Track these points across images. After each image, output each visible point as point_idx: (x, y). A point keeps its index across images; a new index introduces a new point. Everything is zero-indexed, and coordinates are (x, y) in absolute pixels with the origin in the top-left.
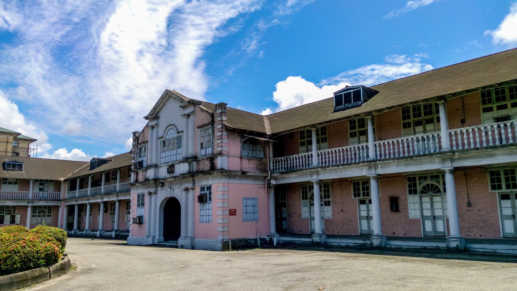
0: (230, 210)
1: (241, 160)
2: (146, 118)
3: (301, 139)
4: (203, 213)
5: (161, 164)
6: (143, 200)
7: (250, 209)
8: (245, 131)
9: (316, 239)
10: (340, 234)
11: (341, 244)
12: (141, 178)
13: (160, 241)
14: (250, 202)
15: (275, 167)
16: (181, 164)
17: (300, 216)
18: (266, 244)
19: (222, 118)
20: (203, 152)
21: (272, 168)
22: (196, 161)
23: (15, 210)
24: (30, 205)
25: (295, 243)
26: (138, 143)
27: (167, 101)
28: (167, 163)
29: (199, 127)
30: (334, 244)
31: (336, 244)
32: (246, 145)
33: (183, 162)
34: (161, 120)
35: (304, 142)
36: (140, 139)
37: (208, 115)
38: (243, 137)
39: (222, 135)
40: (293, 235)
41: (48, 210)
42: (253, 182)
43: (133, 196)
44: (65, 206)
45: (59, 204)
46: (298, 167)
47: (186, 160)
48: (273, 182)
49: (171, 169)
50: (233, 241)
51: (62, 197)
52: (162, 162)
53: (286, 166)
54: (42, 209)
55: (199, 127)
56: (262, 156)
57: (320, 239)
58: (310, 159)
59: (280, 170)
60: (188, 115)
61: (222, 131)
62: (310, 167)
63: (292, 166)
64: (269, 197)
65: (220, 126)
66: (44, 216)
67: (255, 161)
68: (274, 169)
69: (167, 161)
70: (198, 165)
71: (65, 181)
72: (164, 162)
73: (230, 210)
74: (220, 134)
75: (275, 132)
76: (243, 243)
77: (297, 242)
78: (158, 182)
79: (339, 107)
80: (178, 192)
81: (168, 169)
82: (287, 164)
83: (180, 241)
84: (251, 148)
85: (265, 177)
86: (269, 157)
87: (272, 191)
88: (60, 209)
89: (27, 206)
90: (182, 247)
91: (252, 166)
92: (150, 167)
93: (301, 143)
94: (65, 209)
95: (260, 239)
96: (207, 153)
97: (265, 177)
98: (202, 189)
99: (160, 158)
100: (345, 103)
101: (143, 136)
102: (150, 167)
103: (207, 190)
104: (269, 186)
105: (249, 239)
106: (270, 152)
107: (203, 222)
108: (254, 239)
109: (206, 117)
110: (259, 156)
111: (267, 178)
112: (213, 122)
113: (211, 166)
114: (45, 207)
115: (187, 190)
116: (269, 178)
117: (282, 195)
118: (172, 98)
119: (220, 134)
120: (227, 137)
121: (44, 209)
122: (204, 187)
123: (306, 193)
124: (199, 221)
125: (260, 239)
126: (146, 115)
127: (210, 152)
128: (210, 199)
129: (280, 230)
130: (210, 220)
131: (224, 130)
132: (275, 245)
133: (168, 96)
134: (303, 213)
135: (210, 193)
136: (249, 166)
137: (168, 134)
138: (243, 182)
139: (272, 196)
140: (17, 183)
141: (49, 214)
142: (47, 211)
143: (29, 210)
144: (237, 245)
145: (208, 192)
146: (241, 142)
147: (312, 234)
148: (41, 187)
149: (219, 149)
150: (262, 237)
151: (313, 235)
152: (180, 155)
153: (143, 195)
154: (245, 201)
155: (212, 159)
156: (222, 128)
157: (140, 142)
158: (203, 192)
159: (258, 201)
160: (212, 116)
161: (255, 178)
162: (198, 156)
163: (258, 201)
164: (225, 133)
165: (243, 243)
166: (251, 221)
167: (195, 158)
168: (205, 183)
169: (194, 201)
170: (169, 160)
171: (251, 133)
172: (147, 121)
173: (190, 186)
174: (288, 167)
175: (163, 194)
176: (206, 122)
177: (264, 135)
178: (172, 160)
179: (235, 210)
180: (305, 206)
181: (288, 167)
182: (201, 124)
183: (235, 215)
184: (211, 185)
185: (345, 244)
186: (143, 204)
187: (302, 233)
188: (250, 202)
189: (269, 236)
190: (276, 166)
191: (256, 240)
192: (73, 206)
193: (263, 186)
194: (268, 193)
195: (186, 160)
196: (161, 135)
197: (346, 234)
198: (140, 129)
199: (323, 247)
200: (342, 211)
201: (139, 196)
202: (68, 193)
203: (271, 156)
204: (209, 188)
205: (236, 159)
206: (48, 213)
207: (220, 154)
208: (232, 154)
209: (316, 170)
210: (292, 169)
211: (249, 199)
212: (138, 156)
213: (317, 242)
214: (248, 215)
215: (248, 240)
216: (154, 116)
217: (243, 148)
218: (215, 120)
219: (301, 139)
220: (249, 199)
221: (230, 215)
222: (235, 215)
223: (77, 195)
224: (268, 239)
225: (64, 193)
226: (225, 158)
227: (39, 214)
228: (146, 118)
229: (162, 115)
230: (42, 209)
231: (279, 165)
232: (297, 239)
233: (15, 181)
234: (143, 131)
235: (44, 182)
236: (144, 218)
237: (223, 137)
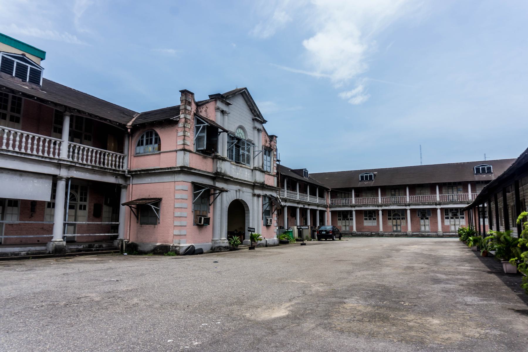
88: (326, 213)
94: (330, 214)
225: (328, 201)
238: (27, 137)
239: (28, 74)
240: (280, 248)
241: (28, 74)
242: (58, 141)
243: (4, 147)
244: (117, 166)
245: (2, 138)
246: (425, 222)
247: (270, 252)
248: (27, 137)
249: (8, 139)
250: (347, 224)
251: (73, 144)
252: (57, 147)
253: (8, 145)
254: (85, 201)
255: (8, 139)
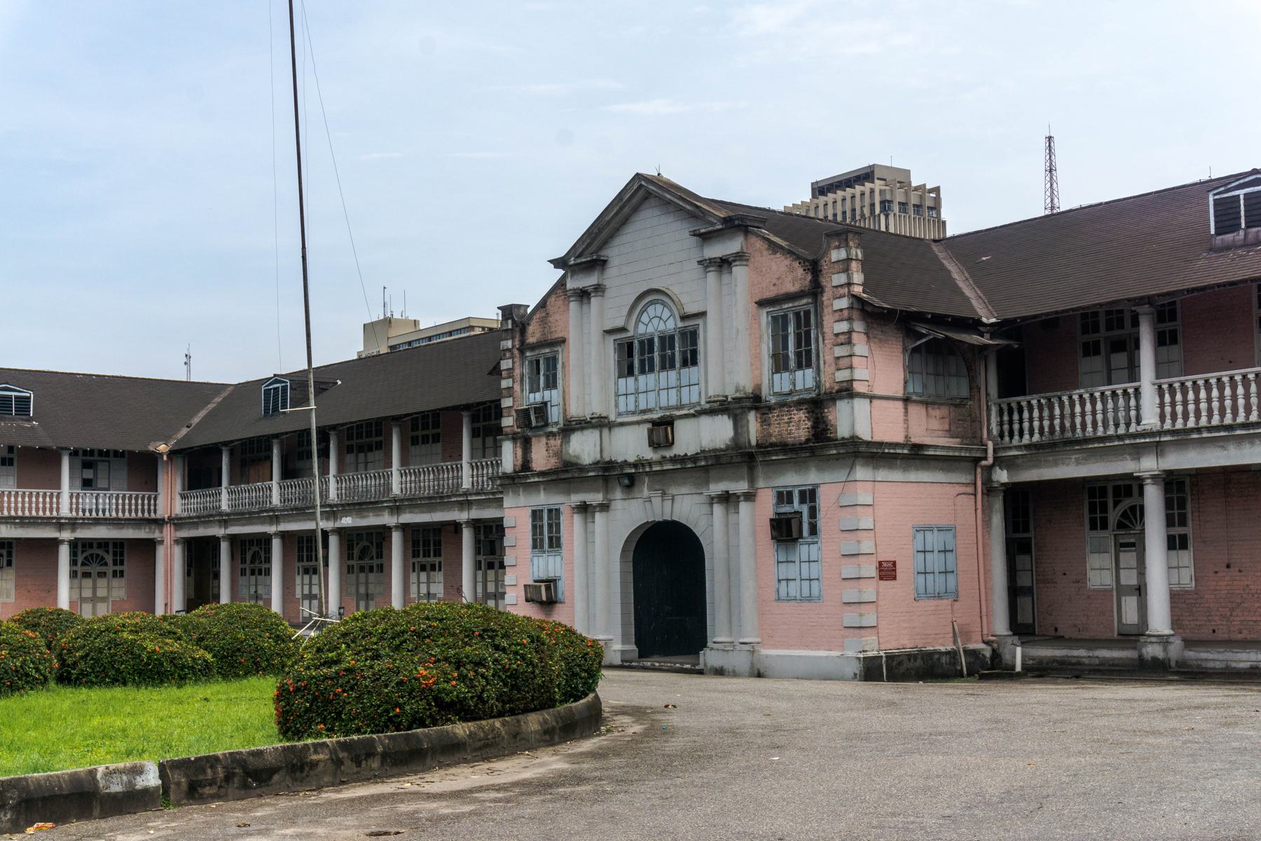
0: (880, 563)
1: (906, 409)
2: (558, 263)
3: (1085, 331)
4: (791, 571)
5: (620, 414)
6: (555, 526)
7: (935, 561)
8: (920, 317)
9: (1152, 651)
10: (1221, 635)
11: (1234, 665)
12: (541, 458)
13: (628, 657)
14: (934, 540)
15: (1006, 427)
16: (705, 421)
17: (1081, 580)
18: (989, 668)
19: (849, 277)
20: (783, 383)
21: (995, 432)
22: (757, 409)
23: (10, 554)
24: (66, 535)
25: (1079, 663)
26: (523, 342)
27: (635, 210)
28: (644, 412)
29: (762, 303)
30: (1211, 665)
31: (1218, 665)
32: (917, 356)
33: (711, 412)
34: (612, 271)
35: (1097, 343)
36: (531, 329)
37: (796, 264)
38: (910, 333)
39: (850, 332)
40: (1057, 639)
41: (115, 554)
42: (940, 476)
43: (516, 513)
44: (177, 542)
45: (156, 535)
46: (1089, 429)
47: (720, 407)
48: (1002, 476)
49: (661, 430)
50: (890, 658)
51: (162, 512)
52: (622, 408)
53: (1046, 423)
54: (96, 551)
55: (762, 303)
56: (965, 392)
57: (1165, 650)
58: (1133, 402)
59: (1027, 436)
60: (724, 264)
61: (850, 319)
62: (1132, 429)
63: (1068, 424)
64: (987, 523)
65: (843, 303)
66: (102, 575)
67: (944, 411)
68: (1001, 435)
69: (642, 406)
70: (765, 422)
71: (172, 453)
72: (631, 407)
73: (880, 563)
74: (843, 327)
75: (1010, 315)
76: (919, 662)
77: (1086, 661)
78: (616, 476)
79: (1229, 237)
80: (687, 506)
81: (650, 432)
82: (1052, 418)
83: (709, 657)
84: (931, 370)
85: (976, 461)
86: (987, 395)
87: (998, 505)
88: (161, 552)
89: (55, 539)
90: (720, 672)
91: (935, 424)
92: (583, 425)
93: (1086, 345)
94: (178, 551)
95: (965, 651)
96: (799, 386)
97: (976, 461)
98: (784, 497)
99: (617, 395)
100: (1248, 227)
101: (544, 322)
102: (583, 425)
103: (802, 501)
104: (989, 489)
105: (935, 652)
106: (990, 381)
107: (789, 599)
108: (948, 653)
109: (792, 270)
110: (954, 393)
111: (984, 463)
112: (815, 291)
113: (814, 427)
114: (103, 544)
115: (727, 499)
116: (990, 461)
117: (1034, 519)
118: (652, 201)
119: (843, 327)
120: (863, 337)
121: (101, 552)
122: (790, 494)
123: (1104, 509)
124: (775, 596)
125: (965, 651)
126: (561, 253)
127: (810, 383)
128: (814, 530)
129: (1021, 629)
130: (815, 592)
131: (856, 314)
132: (1018, 668)
133: (641, 193)
134: (1090, 574)
135: (813, 512)
136: (927, 428)
137: (645, 318)
138: (914, 476)
139: (997, 520)
140: (11, 462)
141: (118, 568)
142: (109, 559)
143: (64, 552)
144: (902, 669)
145: (805, 509)
146: (905, 350)
147: (1134, 636)
148: (89, 474)
149: (842, 375)
150: (971, 646)
151: (1142, 639)
152: (695, 389)
153: (554, 513)
154: (920, 536)
155: (817, 405)
156: (851, 308)
157: (531, 340)
158: (786, 509)
159: (955, 536)
160: (815, 268)
161: (945, 462)
162: (765, 392)
163: (955, 536)
164: (859, 326)
165: (919, 662)
166: (939, 597)
167: (755, 402)
168: (793, 479)
169: (754, 534)
170: (652, 405)
171: (938, 320)
172: (561, 272)
173: (741, 487)
174: (1052, 426)
175: (632, 512)
176: (791, 287)
177: (974, 325)
178: (664, 403)
179: (894, 563)
180: (1100, 550)
181: (1052, 426)
182: (770, 293)
183: (894, 578)
184: (817, 485)
185: (1247, 665)
186: (555, 543)
187: (1086, 635)
188: (934, 540)
189: (987, 643)
190: (1011, 422)
191: (953, 654)
192: (213, 542)
193: (970, 490)
194: (987, 512)
195: (720, 407)
196: (619, 323)
197: (1240, 637)
198: (531, 300)
199: (1177, 673)
200: (1228, 566)
201: (536, 515)
202: (183, 497)
203: (993, 391)
204: (809, 496)
205: (890, 404)
206: (115, 563)
207: (847, 391)
208: (878, 391)
209: (1155, 443)
210: (1069, 434)
211: (931, 529)
212: (527, 387)
213: (1155, 659)
214: (930, 577)
215: (931, 654)
216: (587, 258)
217: (910, 370)
218: (824, 282)
219: (1085, 331)
220: (931, 529)
221: (881, 578)
222: (894, 578)
223: (225, 506)
224: (988, 654)
225: (171, 497)
226: (861, 406)
227: (87, 569)
228: (558, 263)
229: (616, 253)
230: (96, 551)
231: (1021, 421)
232: (1082, 653)
233: (5, 454)
234: (543, 304)
235: (96, 457)
236: (560, 584)
237: (855, 337)
238: (31, 495)
239: (1242, 213)
240: (953, 687)
241: (1242, 213)
242: (55, 492)
243: (6, 513)
244: (1046, 429)
245: (2, 502)
246: (94, 589)
247: (1094, 699)
248: (31, 495)
249: (9, 502)
250: (101, 593)
251: (1165, 382)
252: (1133, 402)
253: (9, 509)
254: (1183, 523)
255: (9, 502)
